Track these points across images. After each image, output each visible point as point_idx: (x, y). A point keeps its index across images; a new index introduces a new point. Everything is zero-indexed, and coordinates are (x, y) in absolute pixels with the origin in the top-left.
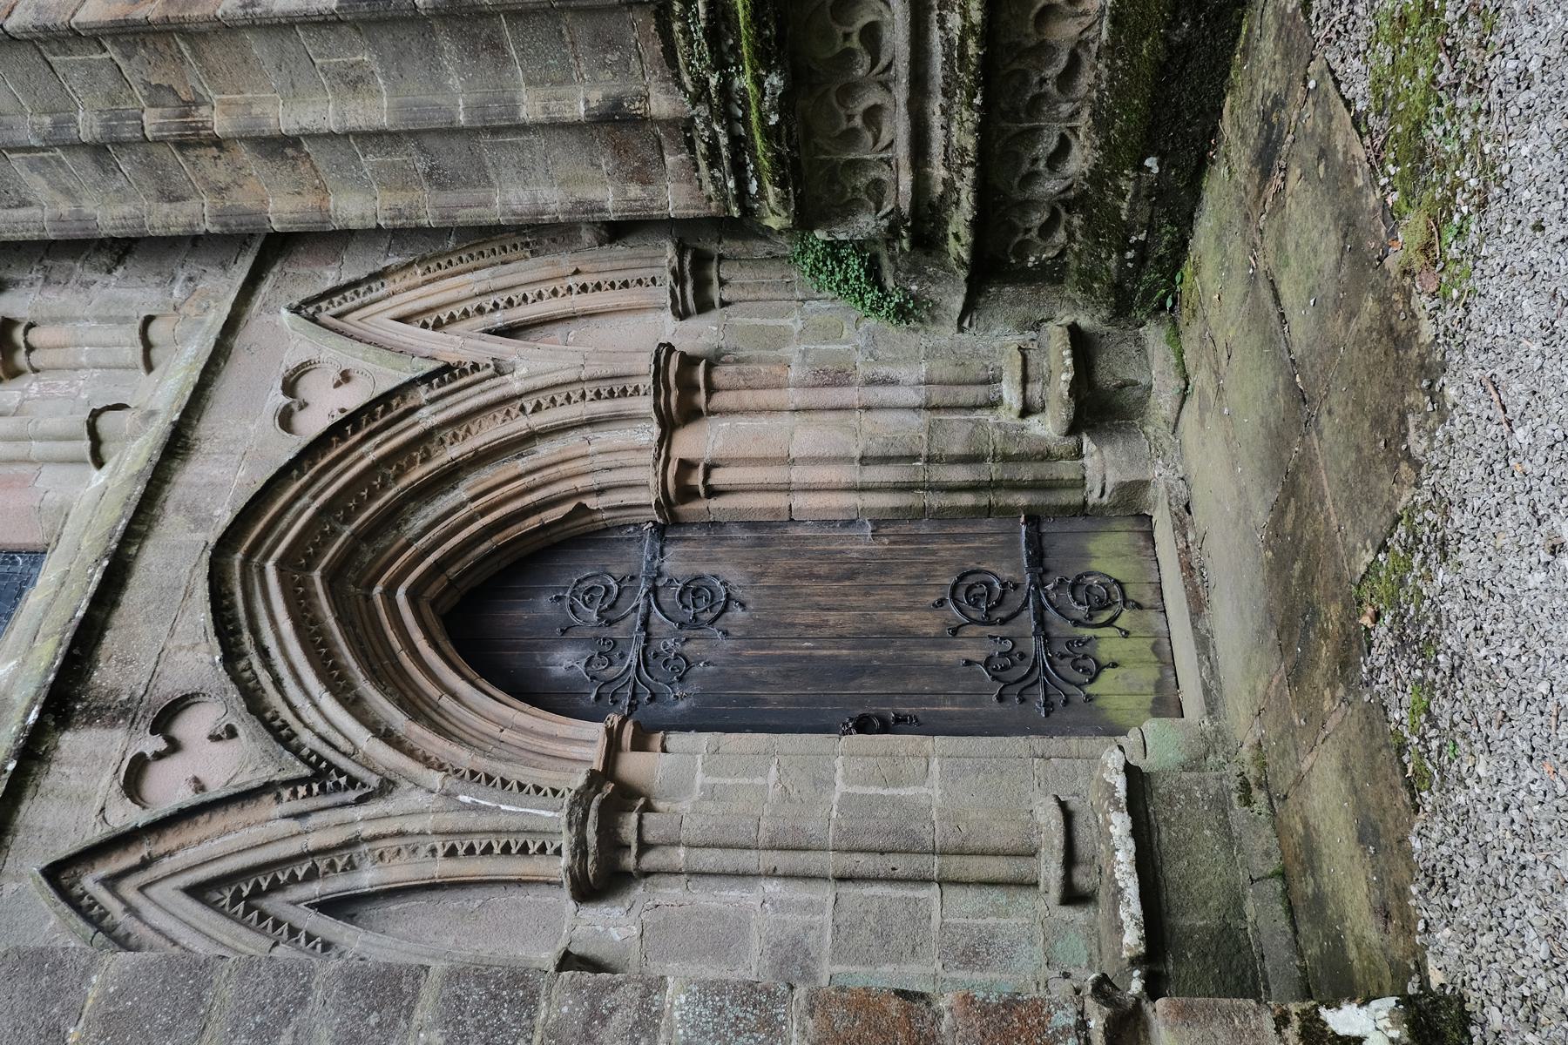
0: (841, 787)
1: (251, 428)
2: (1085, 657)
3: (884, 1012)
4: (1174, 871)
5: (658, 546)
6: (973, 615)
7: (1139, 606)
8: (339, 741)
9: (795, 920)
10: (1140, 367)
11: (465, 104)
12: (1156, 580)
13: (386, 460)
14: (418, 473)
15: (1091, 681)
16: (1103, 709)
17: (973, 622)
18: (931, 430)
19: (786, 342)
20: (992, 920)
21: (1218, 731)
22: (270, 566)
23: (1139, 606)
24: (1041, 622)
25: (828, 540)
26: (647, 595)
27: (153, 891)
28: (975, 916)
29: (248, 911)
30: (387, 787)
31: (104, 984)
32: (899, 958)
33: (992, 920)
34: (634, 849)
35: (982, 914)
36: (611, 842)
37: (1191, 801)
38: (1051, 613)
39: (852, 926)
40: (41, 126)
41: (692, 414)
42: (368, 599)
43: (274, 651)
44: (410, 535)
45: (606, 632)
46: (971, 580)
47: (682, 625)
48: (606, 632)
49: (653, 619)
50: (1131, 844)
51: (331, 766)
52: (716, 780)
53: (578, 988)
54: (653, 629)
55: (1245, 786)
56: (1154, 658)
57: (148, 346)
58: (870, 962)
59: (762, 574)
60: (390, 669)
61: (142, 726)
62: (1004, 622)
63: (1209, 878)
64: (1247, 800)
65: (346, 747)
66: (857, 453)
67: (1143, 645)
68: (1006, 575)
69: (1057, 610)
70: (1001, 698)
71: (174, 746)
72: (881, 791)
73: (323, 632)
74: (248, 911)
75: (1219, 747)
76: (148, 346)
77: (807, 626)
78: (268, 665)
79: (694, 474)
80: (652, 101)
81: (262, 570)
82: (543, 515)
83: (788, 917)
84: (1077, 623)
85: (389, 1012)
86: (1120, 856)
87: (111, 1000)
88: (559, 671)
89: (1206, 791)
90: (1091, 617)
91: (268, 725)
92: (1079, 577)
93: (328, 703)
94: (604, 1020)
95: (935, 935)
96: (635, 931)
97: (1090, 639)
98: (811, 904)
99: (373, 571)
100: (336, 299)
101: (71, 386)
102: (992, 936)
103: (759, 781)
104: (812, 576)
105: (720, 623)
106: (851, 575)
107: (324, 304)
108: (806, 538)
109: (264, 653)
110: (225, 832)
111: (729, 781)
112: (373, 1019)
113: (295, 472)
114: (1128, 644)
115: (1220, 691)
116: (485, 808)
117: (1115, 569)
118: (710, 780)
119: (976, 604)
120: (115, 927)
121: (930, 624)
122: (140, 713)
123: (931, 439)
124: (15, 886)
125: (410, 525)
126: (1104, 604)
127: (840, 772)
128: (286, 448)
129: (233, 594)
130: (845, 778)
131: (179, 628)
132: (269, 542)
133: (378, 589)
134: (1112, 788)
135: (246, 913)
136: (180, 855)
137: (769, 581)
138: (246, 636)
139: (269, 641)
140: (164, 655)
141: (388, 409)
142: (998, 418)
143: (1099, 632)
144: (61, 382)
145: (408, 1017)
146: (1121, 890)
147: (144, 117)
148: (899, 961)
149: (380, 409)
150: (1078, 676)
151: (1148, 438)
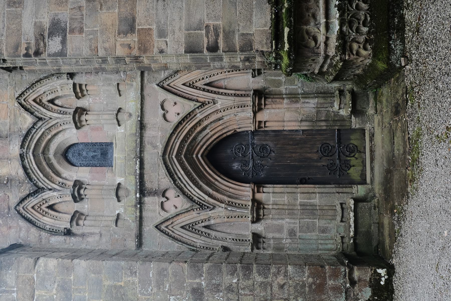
0: (299, 200)
1: (158, 120)
2: (348, 164)
3: (319, 270)
4: (360, 221)
5: (253, 137)
6: (325, 154)
7: (360, 152)
8: (202, 198)
9: (292, 226)
10: (367, 104)
11: (209, 58)
12: (364, 145)
13: (192, 128)
14: (199, 129)
15: (349, 170)
16: (350, 176)
17: (325, 156)
18: (317, 113)
19: (281, 85)
20: (327, 225)
21: (372, 188)
22: (173, 157)
23: (360, 152)
24: (339, 156)
25: (292, 135)
26: (252, 150)
27: (174, 227)
28: (324, 224)
29: (192, 229)
30: (214, 207)
31: (206, 268)
32: (311, 232)
33: (327, 225)
34: (262, 216)
35: (325, 224)
36: (258, 215)
37: (365, 208)
38: (341, 154)
39: (302, 226)
40: (99, 61)
41: (260, 109)
42: (193, 157)
43: (182, 178)
44: (198, 142)
45: (244, 159)
46: (324, 146)
47: (261, 157)
48: (244, 159)
49: (254, 156)
50: (353, 218)
51: (203, 204)
52: (275, 199)
53: (276, 268)
54: (254, 158)
55: (375, 206)
56: (362, 164)
57: (119, 91)
58: (306, 233)
59: (277, 144)
60: (202, 175)
61: (160, 196)
62: (331, 156)
63: (366, 222)
64: (375, 209)
65: (203, 199)
66: (300, 119)
67: (360, 161)
68: (332, 144)
69: (342, 153)
70: (330, 174)
71: (168, 199)
72: (307, 201)
73: (189, 171)
74: (192, 229)
75: (372, 191)
76: (119, 91)
77: (288, 157)
78: (182, 182)
79: (262, 124)
80: (257, 58)
81: (172, 158)
82: (227, 134)
83: (291, 225)
84: (347, 156)
85: (249, 271)
86: (351, 220)
87: (208, 270)
88: (235, 168)
89: (368, 206)
90: (350, 155)
91: (187, 196)
92: (348, 145)
93: (196, 189)
94: (280, 272)
95: (317, 228)
96: (263, 228)
97: (349, 160)
98: (295, 223)
99: (192, 151)
100: (167, 80)
101: (100, 99)
102: (327, 228)
103: (283, 199)
104: (289, 144)
105: (269, 156)
106: (297, 144)
107: (164, 82)
108: (287, 134)
109: (180, 178)
110: (185, 217)
111: (277, 199)
112: (247, 272)
113: (173, 134)
114: (357, 161)
115: (374, 180)
116: (234, 210)
117: (355, 143)
118: (274, 199)
119: (325, 152)
120: (171, 235)
121: (315, 156)
122: (159, 193)
123: (317, 115)
124: (148, 228)
125: (198, 139)
126: (353, 152)
127: (299, 197)
128: (169, 128)
129: (169, 166)
130: (300, 198)
131: (160, 174)
132: (172, 151)
133: (194, 156)
134: (351, 207)
135: (192, 229)
136: (177, 221)
137: (279, 146)
138: (175, 176)
139: (180, 176)
140: (159, 180)
141: (190, 115)
142: (333, 109)
143: (351, 158)
144: (97, 98)
145: (252, 272)
146: (351, 226)
147: (126, 59)
148: (311, 232)
149: (188, 116)
150: (346, 169)
151: (367, 116)
